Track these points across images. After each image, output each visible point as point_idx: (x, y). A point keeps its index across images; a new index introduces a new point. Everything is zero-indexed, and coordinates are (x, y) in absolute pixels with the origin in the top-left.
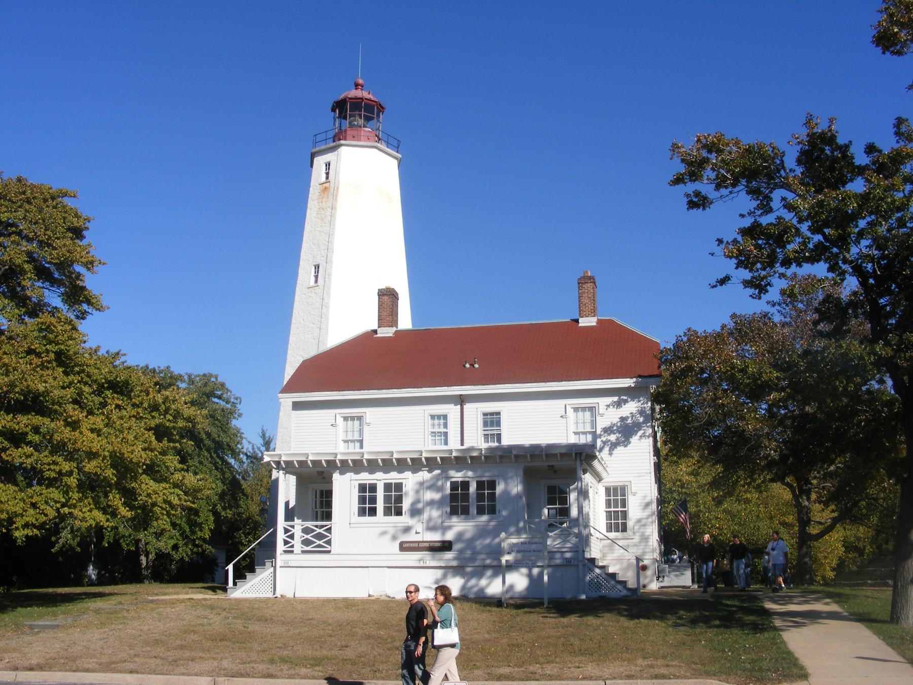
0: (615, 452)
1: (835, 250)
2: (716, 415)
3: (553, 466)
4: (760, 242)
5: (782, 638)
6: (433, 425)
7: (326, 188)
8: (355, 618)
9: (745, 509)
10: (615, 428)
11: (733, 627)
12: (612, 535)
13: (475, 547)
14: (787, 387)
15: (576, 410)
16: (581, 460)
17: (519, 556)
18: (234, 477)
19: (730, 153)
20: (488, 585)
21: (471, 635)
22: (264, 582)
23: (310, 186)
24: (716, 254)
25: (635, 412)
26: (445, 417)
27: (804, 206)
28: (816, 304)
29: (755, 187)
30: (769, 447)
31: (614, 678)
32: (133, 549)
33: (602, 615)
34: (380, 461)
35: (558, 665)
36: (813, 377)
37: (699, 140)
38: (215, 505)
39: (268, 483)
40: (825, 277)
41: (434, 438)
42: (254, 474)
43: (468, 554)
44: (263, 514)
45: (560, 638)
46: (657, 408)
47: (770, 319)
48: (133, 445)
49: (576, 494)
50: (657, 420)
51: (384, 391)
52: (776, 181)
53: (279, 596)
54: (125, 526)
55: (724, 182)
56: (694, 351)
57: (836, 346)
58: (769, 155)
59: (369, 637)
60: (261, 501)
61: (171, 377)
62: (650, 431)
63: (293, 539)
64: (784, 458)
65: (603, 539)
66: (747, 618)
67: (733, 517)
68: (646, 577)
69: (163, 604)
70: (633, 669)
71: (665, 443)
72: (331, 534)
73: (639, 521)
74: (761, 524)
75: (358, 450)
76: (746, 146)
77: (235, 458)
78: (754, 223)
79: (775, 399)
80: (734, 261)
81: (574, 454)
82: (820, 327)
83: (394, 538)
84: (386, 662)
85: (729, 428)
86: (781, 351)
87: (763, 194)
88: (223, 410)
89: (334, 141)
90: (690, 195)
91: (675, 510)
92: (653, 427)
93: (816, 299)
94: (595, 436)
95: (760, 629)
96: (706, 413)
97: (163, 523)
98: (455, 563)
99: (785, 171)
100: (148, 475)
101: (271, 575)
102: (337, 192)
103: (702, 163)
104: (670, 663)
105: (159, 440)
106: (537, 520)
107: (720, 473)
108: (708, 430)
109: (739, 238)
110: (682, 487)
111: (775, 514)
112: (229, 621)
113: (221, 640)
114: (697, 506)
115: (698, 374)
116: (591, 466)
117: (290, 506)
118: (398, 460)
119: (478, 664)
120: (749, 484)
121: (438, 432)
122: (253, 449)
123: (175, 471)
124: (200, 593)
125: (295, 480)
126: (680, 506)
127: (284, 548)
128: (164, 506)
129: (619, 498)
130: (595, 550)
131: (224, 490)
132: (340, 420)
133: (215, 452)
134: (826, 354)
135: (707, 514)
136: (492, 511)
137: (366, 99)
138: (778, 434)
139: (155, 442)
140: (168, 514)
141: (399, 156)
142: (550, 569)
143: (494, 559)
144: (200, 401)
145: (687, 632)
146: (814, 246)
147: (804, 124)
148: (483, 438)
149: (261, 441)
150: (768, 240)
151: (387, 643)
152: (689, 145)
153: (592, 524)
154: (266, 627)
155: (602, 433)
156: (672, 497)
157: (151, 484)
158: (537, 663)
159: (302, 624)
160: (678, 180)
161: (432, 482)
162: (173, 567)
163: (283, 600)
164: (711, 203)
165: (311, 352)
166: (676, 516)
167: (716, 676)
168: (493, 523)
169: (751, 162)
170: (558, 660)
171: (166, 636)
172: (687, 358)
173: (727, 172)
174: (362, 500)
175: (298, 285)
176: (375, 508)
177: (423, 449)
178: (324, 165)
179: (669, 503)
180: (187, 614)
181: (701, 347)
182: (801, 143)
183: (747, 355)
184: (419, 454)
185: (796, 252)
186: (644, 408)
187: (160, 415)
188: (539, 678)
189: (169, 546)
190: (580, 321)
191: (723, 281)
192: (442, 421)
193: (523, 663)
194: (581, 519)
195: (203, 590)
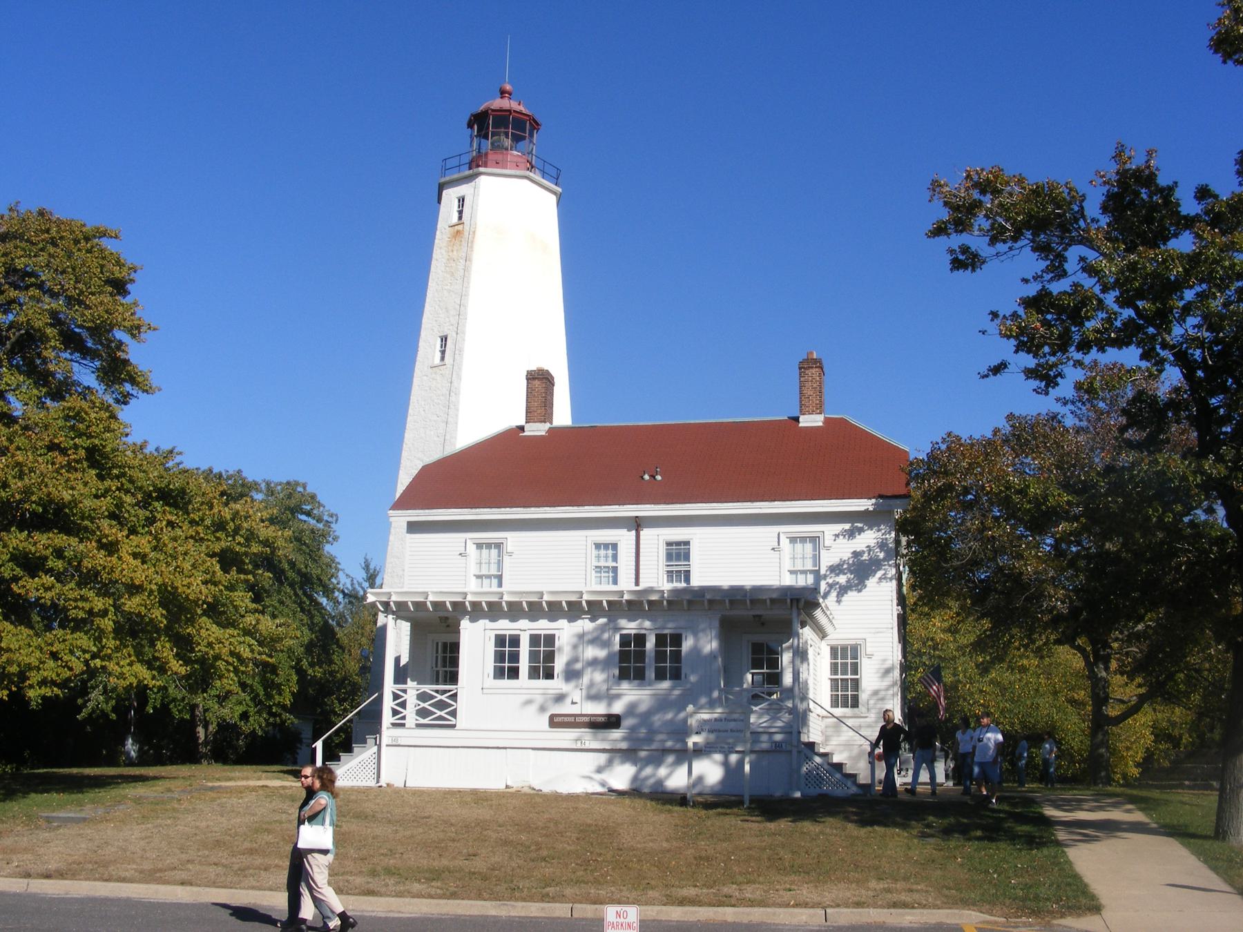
0: (845, 598)
1: (1151, 330)
2: (983, 550)
3: (760, 616)
4: (1049, 317)
5: (1067, 857)
6: (598, 557)
7: (458, 232)
9: (1020, 680)
10: (845, 566)
11: (1000, 840)
12: (839, 711)
14: (1081, 516)
15: (793, 540)
18: (326, 622)
20: (669, 776)
22: (365, 765)
23: (436, 229)
25: (873, 545)
27: (1109, 270)
28: (1123, 403)
29: (1043, 242)
30: (1054, 597)
31: (838, 906)
32: (187, 717)
33: (823, 820)
36: (1117, 502)
37: (968, 177)
38: (299, 660)
40: (1136, 367)
41: (599, 575)
42: (353, 620)
44: (365, 673)
46: (904, 540)
47: (1060, 422)
48: (190, 577)
49: (791, 655)
50: (903, 556)
51: (533, 509)
52: (1073, 234)
54: (176, 686)
55: (1002, 234)
57: (1150, 461)
58: (1064, 199)
59: (506, 843)
61: (243, 485)
62: (894, 571)
64: (1074, 612)
65: (827, 717)
66: (1019, 828)
69: (227, 793)
71: (913, 588)
72: (456, 701)
73: (876, 693)
74: (1041, 701)
75: (495, 589)
77: (328, 597)
78: (1041, 290)
79: (1065, 531)
80: (1013, 342)
81: (789, 601)
83: (542, 709)
85: (1001, 569)
86: (1074, 466)
87: (1055, 251)
88: (313, 531)
89: (470, 169)
92: (897, 566)
93: (1123, 397)
94: (818, 576)
95: (1037, 843)
96: (970, 548)
97: (229, 682)
98: (624, 745)
99: (1085, 221)
100: (209, 617)
104: (915, 887)
105: (226, 570)
107: (986, 630)
109: (1021, 311)
110: (935, 648)
111: (1061, 687)
114: (955, 675)
115: (960, 494)
116: (812, 617)
118: (549, 603)
119: (653, 882)
120: (1026, 646)
122: (352, 584)
123: (246, 612)
124: (278, 779)
125: (409, 628)
127: (393, 720)
128: (230, 660)
130: (815, 732)
131: (311, 640)
132: (472, 548)
134: (1135, 472)
135: (968, 686)
136: (676, 675)
137: (514, 111)
138: (1067, 579)
139: (219, 573)
140: (236, 671)
141: (560, 190)
142: (753, 756)
143: (678, 741)
144: (281, 518)
145: (938, 845)
146: (1123, 324)
148: (665, 576)
150: (1059, 314)
152: (955, 183)
153: (811, 695)
155: (828, 573)
157: (213, 630)
158: (733, 883)
160: (939, 230)
161: (595, 634)
162: (241, 742)
164: (984, 262)
166: (926, 687)
167: (977, 905)
168: (677, 692)
169: (1039, 208)
171: (230, 835)
172: (946, 473)
174: (500, 657)
175: (417, 363)
178: (457, 201)
182: (1108, 183)
184: (578, 596)
185: (1097, 331)
186: (886, 539)
187: (227, 536)
189: (237, 715)
190: (801, 419)
191: (998, 369)
192: (610, 552)
193: (715, 882)
194: (796, 689)
195: (281, 774)
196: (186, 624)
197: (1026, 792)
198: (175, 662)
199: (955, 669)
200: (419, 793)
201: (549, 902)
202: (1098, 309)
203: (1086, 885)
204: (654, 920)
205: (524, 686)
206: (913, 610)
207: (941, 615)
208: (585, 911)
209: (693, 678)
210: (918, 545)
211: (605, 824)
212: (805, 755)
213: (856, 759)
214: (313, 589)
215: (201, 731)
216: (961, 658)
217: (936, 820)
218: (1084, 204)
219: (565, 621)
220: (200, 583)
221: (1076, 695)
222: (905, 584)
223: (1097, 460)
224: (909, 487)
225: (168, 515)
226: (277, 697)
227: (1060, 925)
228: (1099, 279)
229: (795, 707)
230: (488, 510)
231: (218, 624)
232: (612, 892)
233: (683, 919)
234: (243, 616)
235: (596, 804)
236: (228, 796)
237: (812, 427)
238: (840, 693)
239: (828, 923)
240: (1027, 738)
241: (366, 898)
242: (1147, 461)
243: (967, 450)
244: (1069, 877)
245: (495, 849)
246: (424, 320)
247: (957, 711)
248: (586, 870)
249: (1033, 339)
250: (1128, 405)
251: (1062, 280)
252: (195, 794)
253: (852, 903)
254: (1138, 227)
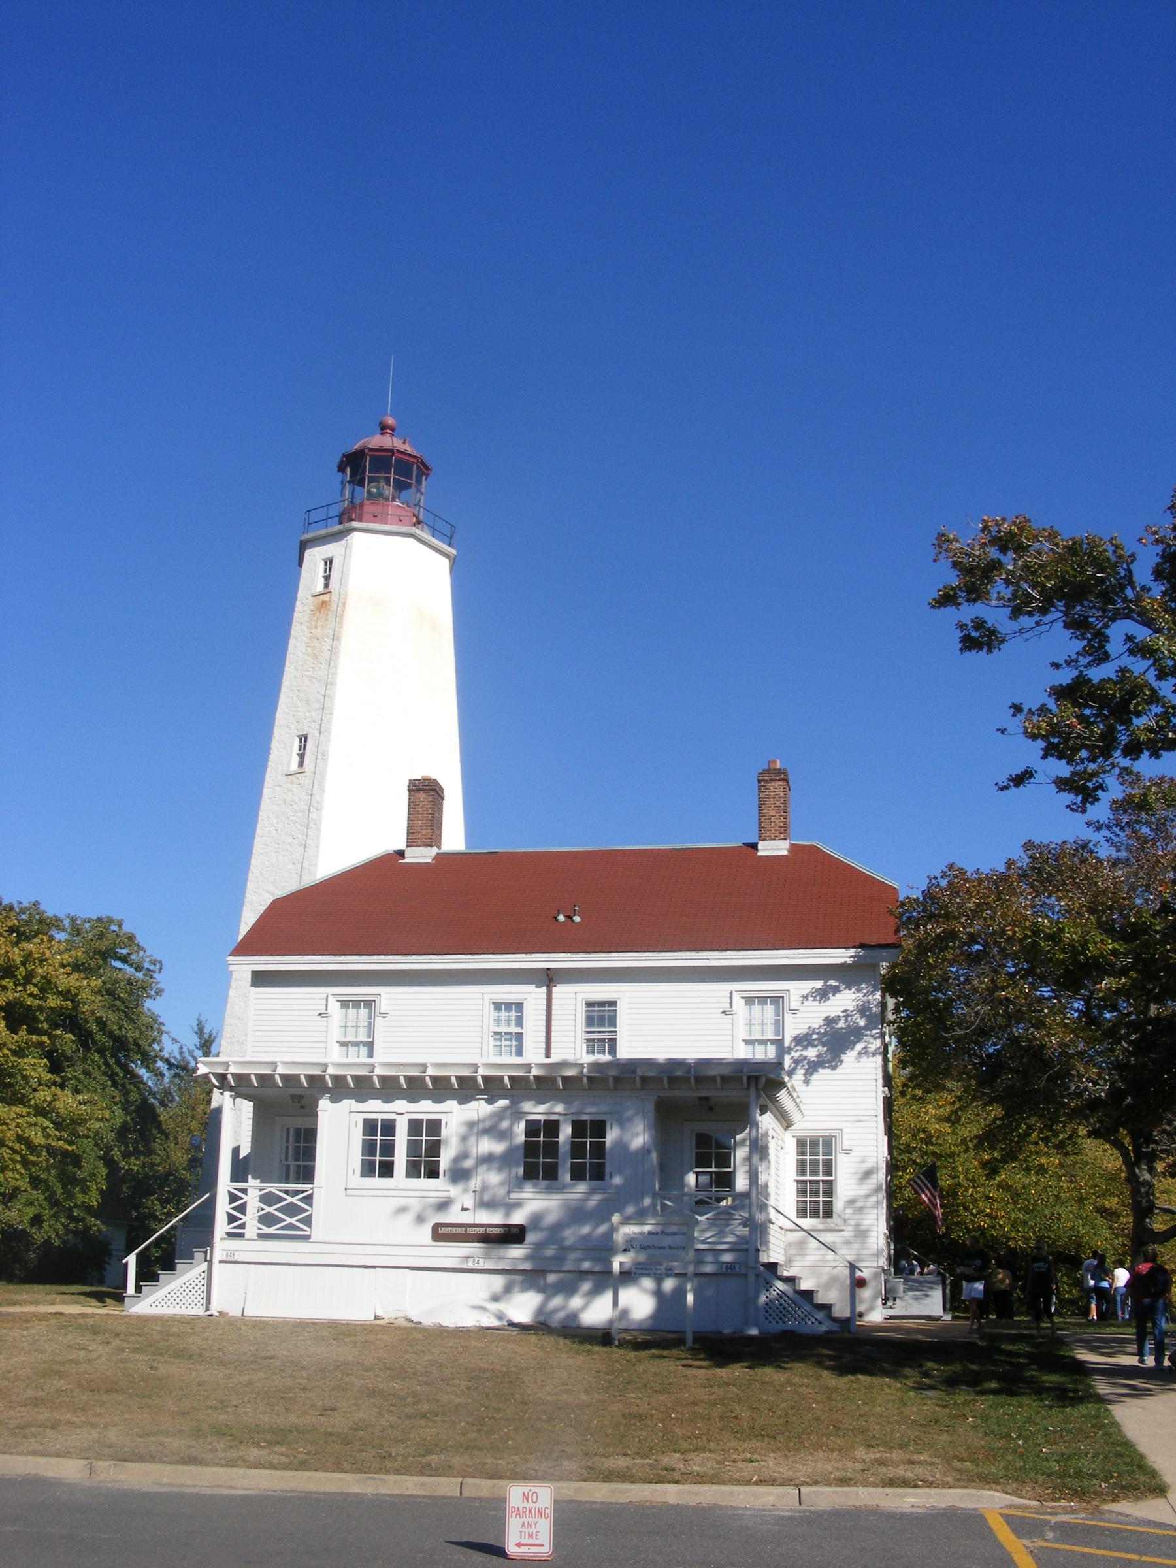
0: (815, 1077)
3: (707, 1099)
4: (1087, 712)
5: (1113, 1417)
6: (498, 1020)
7: (323, 603)
8: (350, 1358)
11: (1024, 1394)
12: (807, 1223)
13: (563, 1240)
14: (1131, 969)
15: (749, 1001)
16: (757, 1090)
17: (642, 1257)
18: (145, 1101)
20: (585, 1307)
22: (190, 1287)
23: (296, 599)
24: (1009, 731)
25: (851, 1008)
26: (519, 1006)
29: (1080, 615)
31: (816, 1483)
35: (713, 1456)
37: (985, 528)
38: (109, 1149)
39: (205, 1114)
41: (498, 1043)
42: (180, 1098)
44: (195, 1167)
45: (715, 1405)
46: (891, 1003)
49: (747, 1149)
50: (890, 1023)
53: (217, 1314)
55: (1027, 604)
58: (1108, 559)
59: (374, 1393)
60: (192, 1145)
61: (40, 921)
62: (878, 1043)
64: (1116, 1095)
66: (1046, 1378)
67: (1016, 1196)
70: (850, 1467)
71: (903, 1063)
72: (311, 1205)
73: (851, 1202)
74: (1063, 1211)
75: (364, 1059)
76: (1067, 541)
77: (147, 1067)
78: (1077, 677)
79: (1109, 989)
80: (1041, 744)
81: (745, 1079)
83: (420, 1219)
84: (403, 1441)
85: (1015, 1041)
86: (1111, 908)
87: (1093, 628)
88: (129, 983)
89: (340, 523)
90: (966, 625)
91: (915, 1182)
94: (782, 1050)
95: (1072, 1399)
96: (977, 1013)
98: (526, 1266)
99: (1133, 588)
101: (203, 1275)
104: (916, 1457)
107: (995, 1119)
108: (976, 1043)
109: (1051, 704)
111: (1088, 1193)
112: (124, 1355)
113: (107, 1392)
116: (775, 1101)
118: (434, 1079)
119: (569, 1449)
120: (1046, 1140)
121: (506, 1033)
122: (181, 1053)
123: (40, 1085)
125: (251, 1110)
126: (924, 1176)
127: (228, 1229)
128: (17, 1146)
130: (775, 1252)
131: (125, 1123)
132: (335, 1007)
136: (598, 1174)
137: (398, 451)
140: (25, 1162)
141: (454, 552)
142: (696, 1281)
143: (595, 1260)
144: (89, 964)
145: (941, 1399)
147: (1169, 508)
148: (585, 1046)
151: (405, 1406)
158: (675, 1451)
160: (947, 599)
161: (488, 1124)
163: (222, 1321)
164: (1003, 641)
165: (288, 886)
166: (916, 1193)
167: (1000, 1484)
169: (1075, 570)
170: (712, 1445)
171: (8, 1380)
172: (948, 916)
173: (1034, 587)
174: (369, 1148)
176: (392, 1163)
177: (479, 1061)
178: (323, 563)
179: (904, 1169)
184: (472, 1069)
187: (16, 985)
188: (680, 1478)
190: (760, 847)
191: (1021, 779)
192: (513, 1014)
193: (651, 1449)
195: (82, 1297)
200: (260, 1325)
201: (431, 1476)
203: (1142, 1457)
204: (572, 1501)
208: (480, 1487)
211: (504, 1369)
214: (129, 1057)
217: (936, 1367)
219: (455, 1103)
221: (1107, 1203)
222: (891, 1059)
226: (80, 1196)
227: (1112, 1512)
228: (1156, 661)
232: (515, 1463)
233: (608, 1500)
234: (35, 1090)
236: (9, 1325)
239: (803, 1507)
241: (186, 1468)
243: (974, 886)
244: (1118, 1445)
245: (360, 1402)
247: (957, 1224)
248: (479, 1431)
249: (1067, 739)
251: (1103, 665)
253: (835, 1479)
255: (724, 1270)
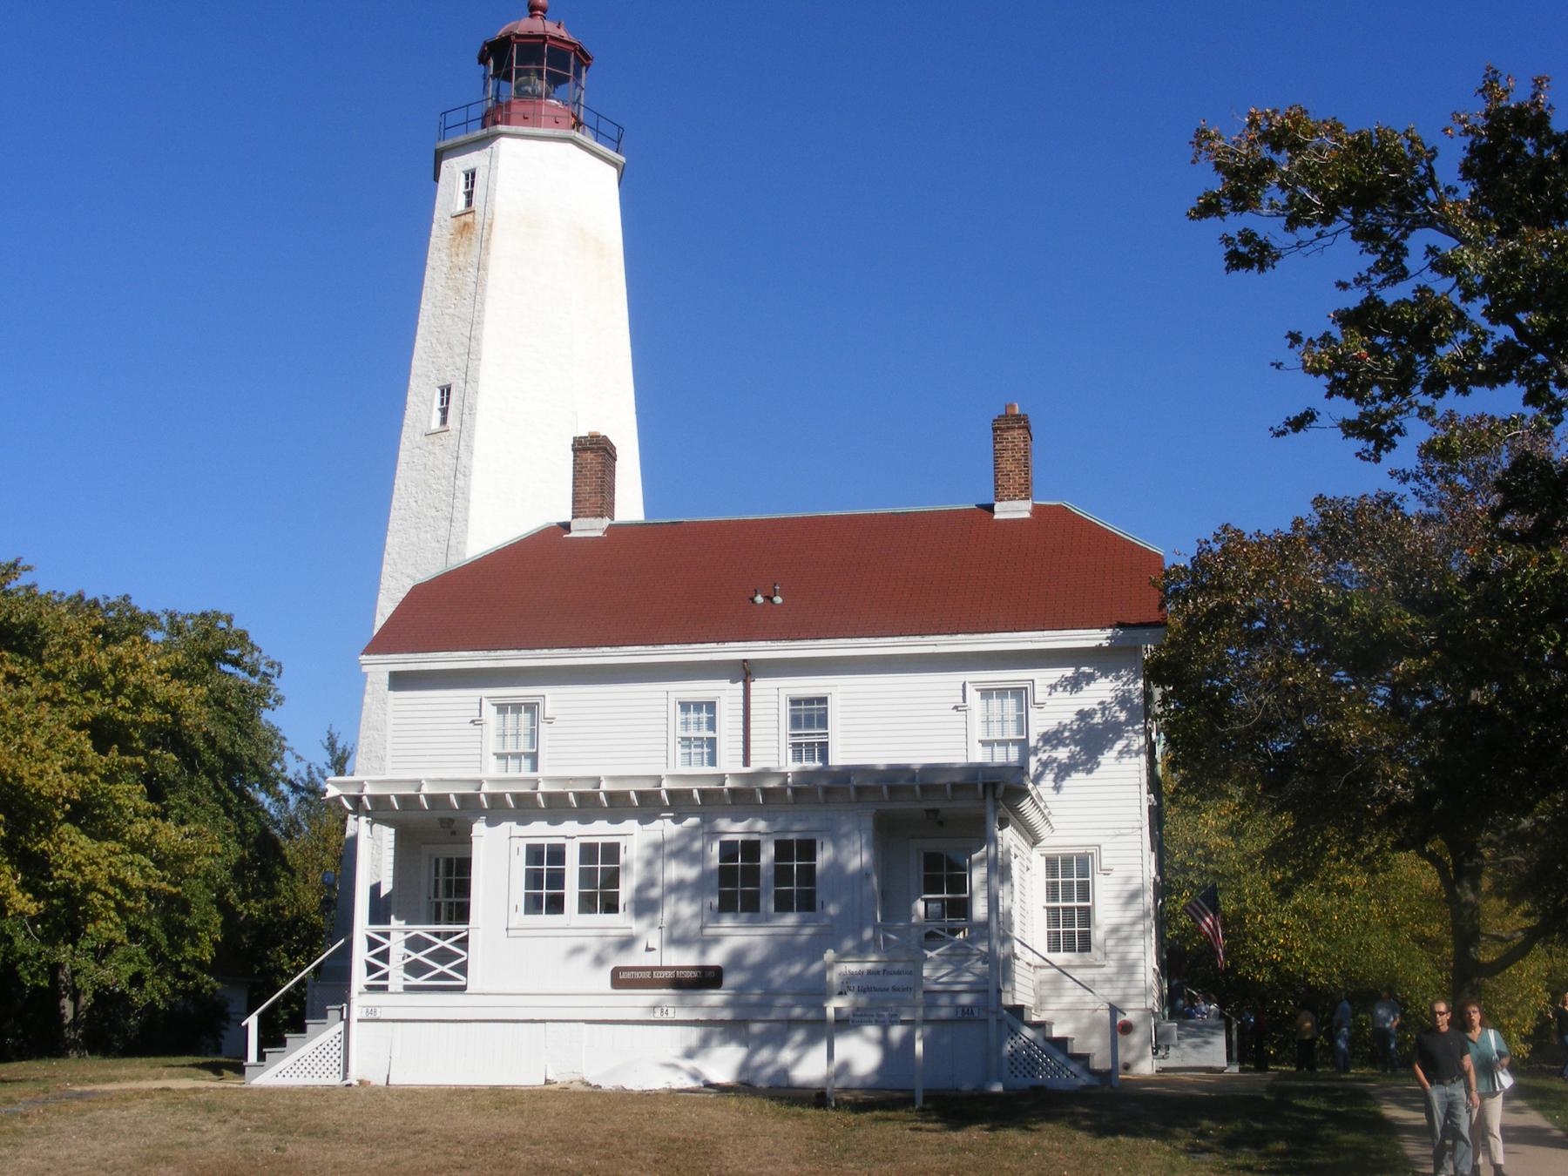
0: (1067, 783)
1: (1540, 358)
2: (1280, 706)
3: (935, 811)
4: (1380, 340)
6: (686, 723)
7: (466, 224)
9: (1339, 907)
10: (1067, 734)
12: (1060, 958)
13: (770, 981)
14: (1433, 648)
15: (986, 694)
16: (995, 799)
17: (863, 1000)
18: (265, 831)
19: (1320, 151)
20: (797, 1061)
21: (760, 1166)
22: (324, 1053)
23: (432, 221)
25: (1109, 700)
26: (711, 706)
27: (1476, 263)
28: (1494, 474)
29: (1371, 224)
30: (1391, 778)
32: (45, 983)
33: (1037, 1127)
34: (571, 796)
36: (1490, 626)
37: (1253, 122)
38: (222, 891)
40: (1518, 415)
41: (687, 751)
43: (755, 995)
44: (328, 910)
46: (1157, 692)
47: (1396, 507)
48: (43, 761)
49: (985, 870)
50: (1156, 717)
51: (583, 650)
52: (1417, 212)
54: (28, 936)
55: (1306, 212)
56: (1234, 572)
57: (1541, 560)
58: (1404, 156)
61: (132, 619)
62: (1142, 740)
63: (387, 960)
64: (1424, 799)
65: (1041, 967)
67: (1315, 923)
68: (1128, 1048)
69: (104, 1100)
71: (1172, 765)
72: (466, 950)
73: (1115, 930)
74: (1372, 939)
75: (527, 773)
77: (267, 791)
78: (1367, 299)
79: (1408, 672)
80: (1324, 380)
81: (980, 787)
82: (1507, 521)
83: (599, 961)
85: (1307, 735)
86: (1420, 575)
87: (1388, 239)
89: (484, 127)
90: (1233, 239)
92: (1147, 733)
93: (1495, 468)
97: (107, 928)
98: (726, 1015)
99: (1436, 190)
100: (75, 823)
101: (339, 1037)
102: (490, 235)
103: (1260, 172)
105: (101, 748)
106: (902, 924)
107: (1286, 832)
109: (1336, 332)
110: (1207, 859)
112: (245, 1135)
114: (1238, 900)
115: (1243, 621)
116: (1017, 813)
117: (383, 893)
118: (610, 795)
120: (1349, 855)
121: (696, 739)
122: (309, 773)
124: (188, 1076)
125: (392, 838)
127: (368, 980)
128: (111, 890)
129: (1075, 879)
130: (1023, 990)
131: (242, 858)
132: (490, 712)
133: (226, 778)
134: (1518, 579)
135: (1260, 917)
136: (808, 904)
137: (552, 37)
138: (1411, 750)
139: (91, 755)
140: (120, 909)
141: (622, 159)
142: (928, 1029)
143: (808, 1006)
144: (193, 669)
146: (1496, 350)
147: (1480, 91)
148: (790, 752)
149: (326, 757)
150: (1396, 336)
152: (1232, 134)
153: (1017, 933)
154: (324, 1149)
155: (1040, 744)
156: (1185, 881)
157: (81, 843)
159: (401, 1143)
160: (1208, 208)
161: (680, 843)
162: (132, 1022)
164: (1277, 257)
165: (431, 568)
166: (1194, 920)
168: (808, 931)
169: (1364, 170)
172: (1221, 588)
173: (1314, 191)
174: (533, 879)
175: (405, 429)
176: (562, 896)
178: (463, 176)
180: (154, 1121)
181: (1250, 564)
182: (1473, 132)
183: (1347, 583)
185: (1457, 361)
186: (1129, 691)
187: (104, 697)
189: (124, 978)
190: (996, 508)
191: (1301, 422)
192: (704, 716)
194: (994, 924)
195: (194, 1070)
196: (38, 834)
197: (1354, 1080)
198: (20, 896)
199: (1239, 891)
200: (410, 1094)
202: (1457, 328)
205: (573, 925)
206: (1173, 801)
207: (1216, 809)
209: (832, 909)
210: (1179, 701)
211: (699, 1138)
212: (1009, 1025)
213: (1087, 1032)
215: (67, 1006)
216: (1249, 874)
218: (1433, 164)
219: (635, 822)
220: (59, 769)
221: (1427, 930)
222: (1159, 760)
223: (1455, 566)
224: (1164, 611)
225: (7, 664)
229: (992, 952)
230: (515, 652)
231: (91, 835)
234: (131, 822)
235: (685, 1106)
236: (106, 1105)
237: (1014, 521)
238: (1061, 929)
240: (1351, 998)
242: (1536, 559)
243: (1253, 551)
246: (415, 362)
247: (1244, 957)
250: (1504, 476)
251: (1401, 285)
252: (52, 1106)
254: (1519, 197)
255: (960, 1015)
